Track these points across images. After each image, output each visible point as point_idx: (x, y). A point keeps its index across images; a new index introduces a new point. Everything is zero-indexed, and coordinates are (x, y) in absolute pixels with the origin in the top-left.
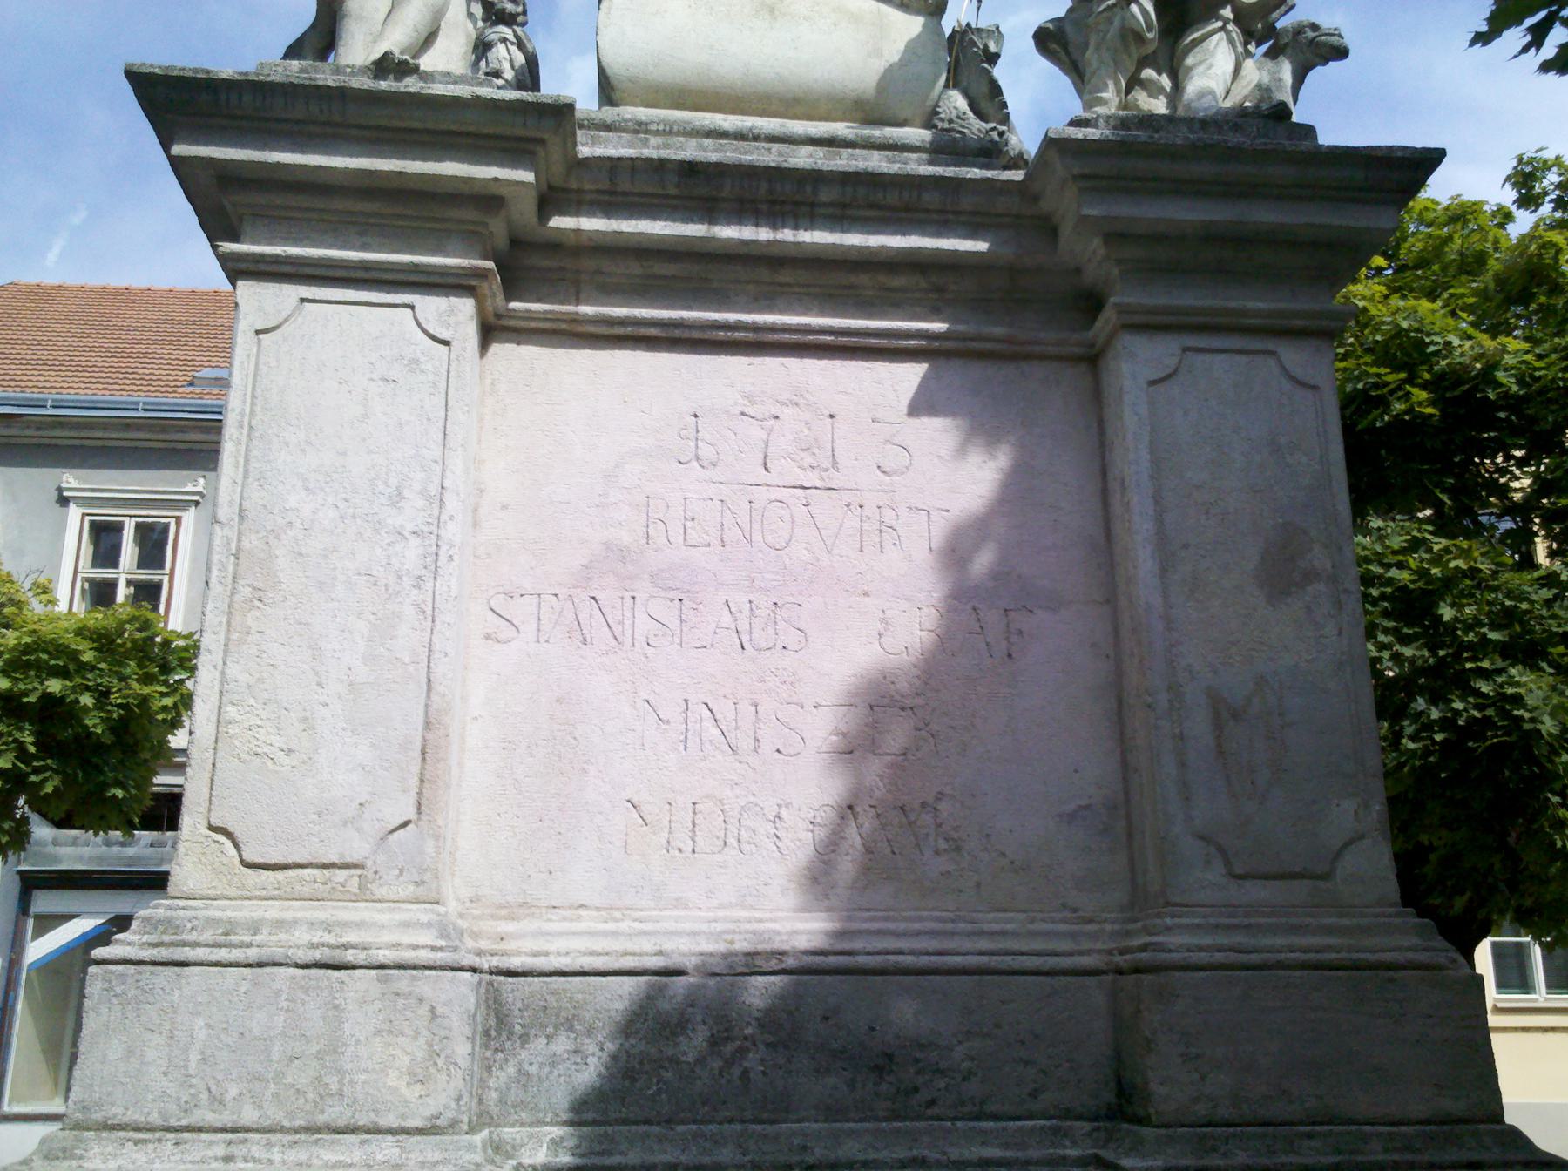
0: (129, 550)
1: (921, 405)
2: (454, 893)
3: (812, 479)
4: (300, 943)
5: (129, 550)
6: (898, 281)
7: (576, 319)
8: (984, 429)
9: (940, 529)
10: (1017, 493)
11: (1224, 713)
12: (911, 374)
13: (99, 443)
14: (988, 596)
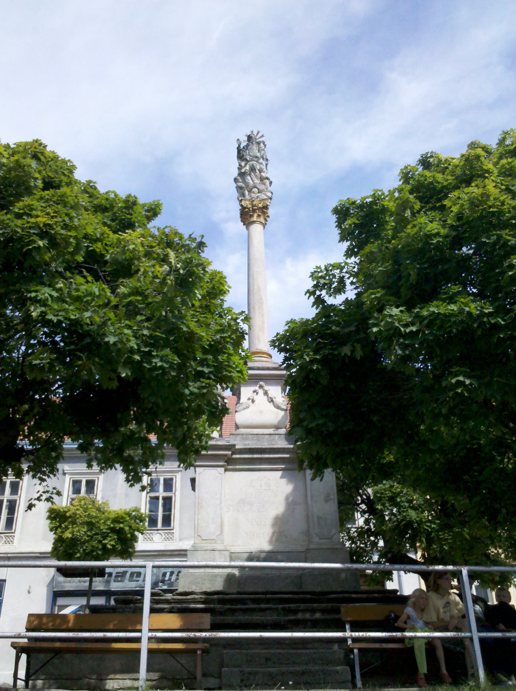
0: (83, 489)
1: (282, 477)
2: (225, 544)
3: (267, 488)
4: (209, 548)
5: (83, 489)
6: (278, 460)
7: (236, 468)
8: (290, 481)
9: (284, 495)
10: (295, 489)
11: (319, 518)
12: (280, 473)
13: (74, 455)
14: (291, 504)
